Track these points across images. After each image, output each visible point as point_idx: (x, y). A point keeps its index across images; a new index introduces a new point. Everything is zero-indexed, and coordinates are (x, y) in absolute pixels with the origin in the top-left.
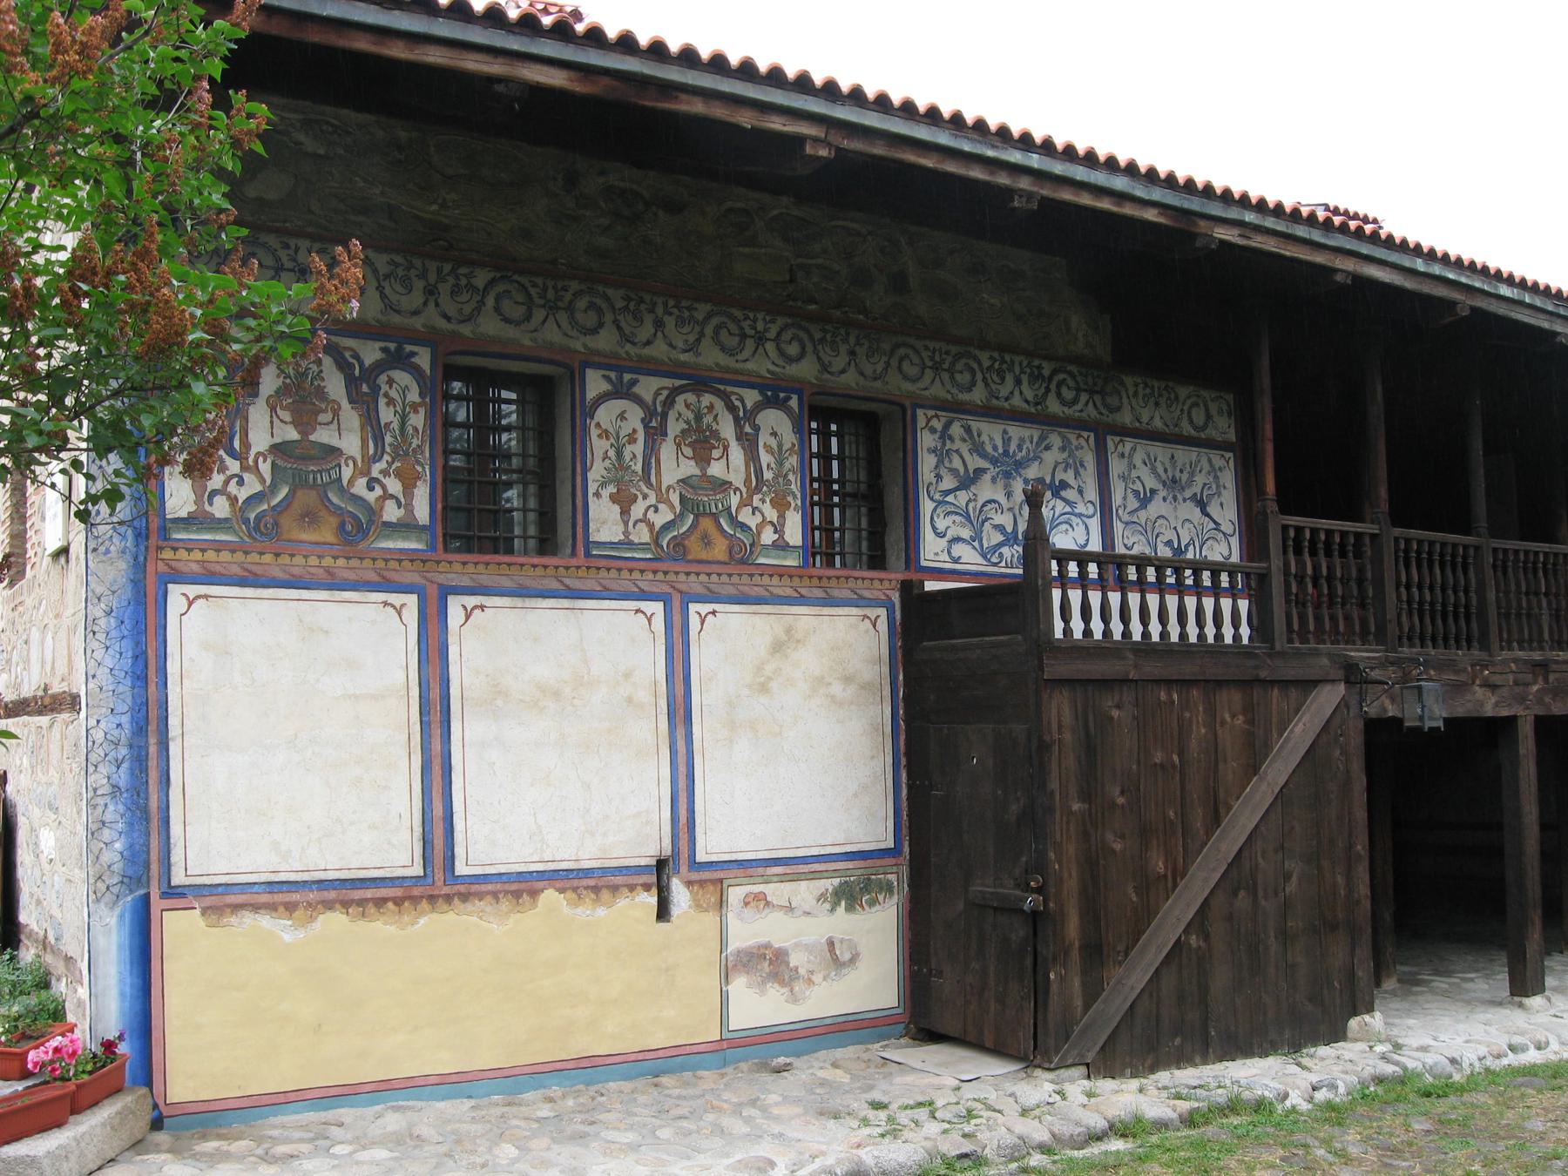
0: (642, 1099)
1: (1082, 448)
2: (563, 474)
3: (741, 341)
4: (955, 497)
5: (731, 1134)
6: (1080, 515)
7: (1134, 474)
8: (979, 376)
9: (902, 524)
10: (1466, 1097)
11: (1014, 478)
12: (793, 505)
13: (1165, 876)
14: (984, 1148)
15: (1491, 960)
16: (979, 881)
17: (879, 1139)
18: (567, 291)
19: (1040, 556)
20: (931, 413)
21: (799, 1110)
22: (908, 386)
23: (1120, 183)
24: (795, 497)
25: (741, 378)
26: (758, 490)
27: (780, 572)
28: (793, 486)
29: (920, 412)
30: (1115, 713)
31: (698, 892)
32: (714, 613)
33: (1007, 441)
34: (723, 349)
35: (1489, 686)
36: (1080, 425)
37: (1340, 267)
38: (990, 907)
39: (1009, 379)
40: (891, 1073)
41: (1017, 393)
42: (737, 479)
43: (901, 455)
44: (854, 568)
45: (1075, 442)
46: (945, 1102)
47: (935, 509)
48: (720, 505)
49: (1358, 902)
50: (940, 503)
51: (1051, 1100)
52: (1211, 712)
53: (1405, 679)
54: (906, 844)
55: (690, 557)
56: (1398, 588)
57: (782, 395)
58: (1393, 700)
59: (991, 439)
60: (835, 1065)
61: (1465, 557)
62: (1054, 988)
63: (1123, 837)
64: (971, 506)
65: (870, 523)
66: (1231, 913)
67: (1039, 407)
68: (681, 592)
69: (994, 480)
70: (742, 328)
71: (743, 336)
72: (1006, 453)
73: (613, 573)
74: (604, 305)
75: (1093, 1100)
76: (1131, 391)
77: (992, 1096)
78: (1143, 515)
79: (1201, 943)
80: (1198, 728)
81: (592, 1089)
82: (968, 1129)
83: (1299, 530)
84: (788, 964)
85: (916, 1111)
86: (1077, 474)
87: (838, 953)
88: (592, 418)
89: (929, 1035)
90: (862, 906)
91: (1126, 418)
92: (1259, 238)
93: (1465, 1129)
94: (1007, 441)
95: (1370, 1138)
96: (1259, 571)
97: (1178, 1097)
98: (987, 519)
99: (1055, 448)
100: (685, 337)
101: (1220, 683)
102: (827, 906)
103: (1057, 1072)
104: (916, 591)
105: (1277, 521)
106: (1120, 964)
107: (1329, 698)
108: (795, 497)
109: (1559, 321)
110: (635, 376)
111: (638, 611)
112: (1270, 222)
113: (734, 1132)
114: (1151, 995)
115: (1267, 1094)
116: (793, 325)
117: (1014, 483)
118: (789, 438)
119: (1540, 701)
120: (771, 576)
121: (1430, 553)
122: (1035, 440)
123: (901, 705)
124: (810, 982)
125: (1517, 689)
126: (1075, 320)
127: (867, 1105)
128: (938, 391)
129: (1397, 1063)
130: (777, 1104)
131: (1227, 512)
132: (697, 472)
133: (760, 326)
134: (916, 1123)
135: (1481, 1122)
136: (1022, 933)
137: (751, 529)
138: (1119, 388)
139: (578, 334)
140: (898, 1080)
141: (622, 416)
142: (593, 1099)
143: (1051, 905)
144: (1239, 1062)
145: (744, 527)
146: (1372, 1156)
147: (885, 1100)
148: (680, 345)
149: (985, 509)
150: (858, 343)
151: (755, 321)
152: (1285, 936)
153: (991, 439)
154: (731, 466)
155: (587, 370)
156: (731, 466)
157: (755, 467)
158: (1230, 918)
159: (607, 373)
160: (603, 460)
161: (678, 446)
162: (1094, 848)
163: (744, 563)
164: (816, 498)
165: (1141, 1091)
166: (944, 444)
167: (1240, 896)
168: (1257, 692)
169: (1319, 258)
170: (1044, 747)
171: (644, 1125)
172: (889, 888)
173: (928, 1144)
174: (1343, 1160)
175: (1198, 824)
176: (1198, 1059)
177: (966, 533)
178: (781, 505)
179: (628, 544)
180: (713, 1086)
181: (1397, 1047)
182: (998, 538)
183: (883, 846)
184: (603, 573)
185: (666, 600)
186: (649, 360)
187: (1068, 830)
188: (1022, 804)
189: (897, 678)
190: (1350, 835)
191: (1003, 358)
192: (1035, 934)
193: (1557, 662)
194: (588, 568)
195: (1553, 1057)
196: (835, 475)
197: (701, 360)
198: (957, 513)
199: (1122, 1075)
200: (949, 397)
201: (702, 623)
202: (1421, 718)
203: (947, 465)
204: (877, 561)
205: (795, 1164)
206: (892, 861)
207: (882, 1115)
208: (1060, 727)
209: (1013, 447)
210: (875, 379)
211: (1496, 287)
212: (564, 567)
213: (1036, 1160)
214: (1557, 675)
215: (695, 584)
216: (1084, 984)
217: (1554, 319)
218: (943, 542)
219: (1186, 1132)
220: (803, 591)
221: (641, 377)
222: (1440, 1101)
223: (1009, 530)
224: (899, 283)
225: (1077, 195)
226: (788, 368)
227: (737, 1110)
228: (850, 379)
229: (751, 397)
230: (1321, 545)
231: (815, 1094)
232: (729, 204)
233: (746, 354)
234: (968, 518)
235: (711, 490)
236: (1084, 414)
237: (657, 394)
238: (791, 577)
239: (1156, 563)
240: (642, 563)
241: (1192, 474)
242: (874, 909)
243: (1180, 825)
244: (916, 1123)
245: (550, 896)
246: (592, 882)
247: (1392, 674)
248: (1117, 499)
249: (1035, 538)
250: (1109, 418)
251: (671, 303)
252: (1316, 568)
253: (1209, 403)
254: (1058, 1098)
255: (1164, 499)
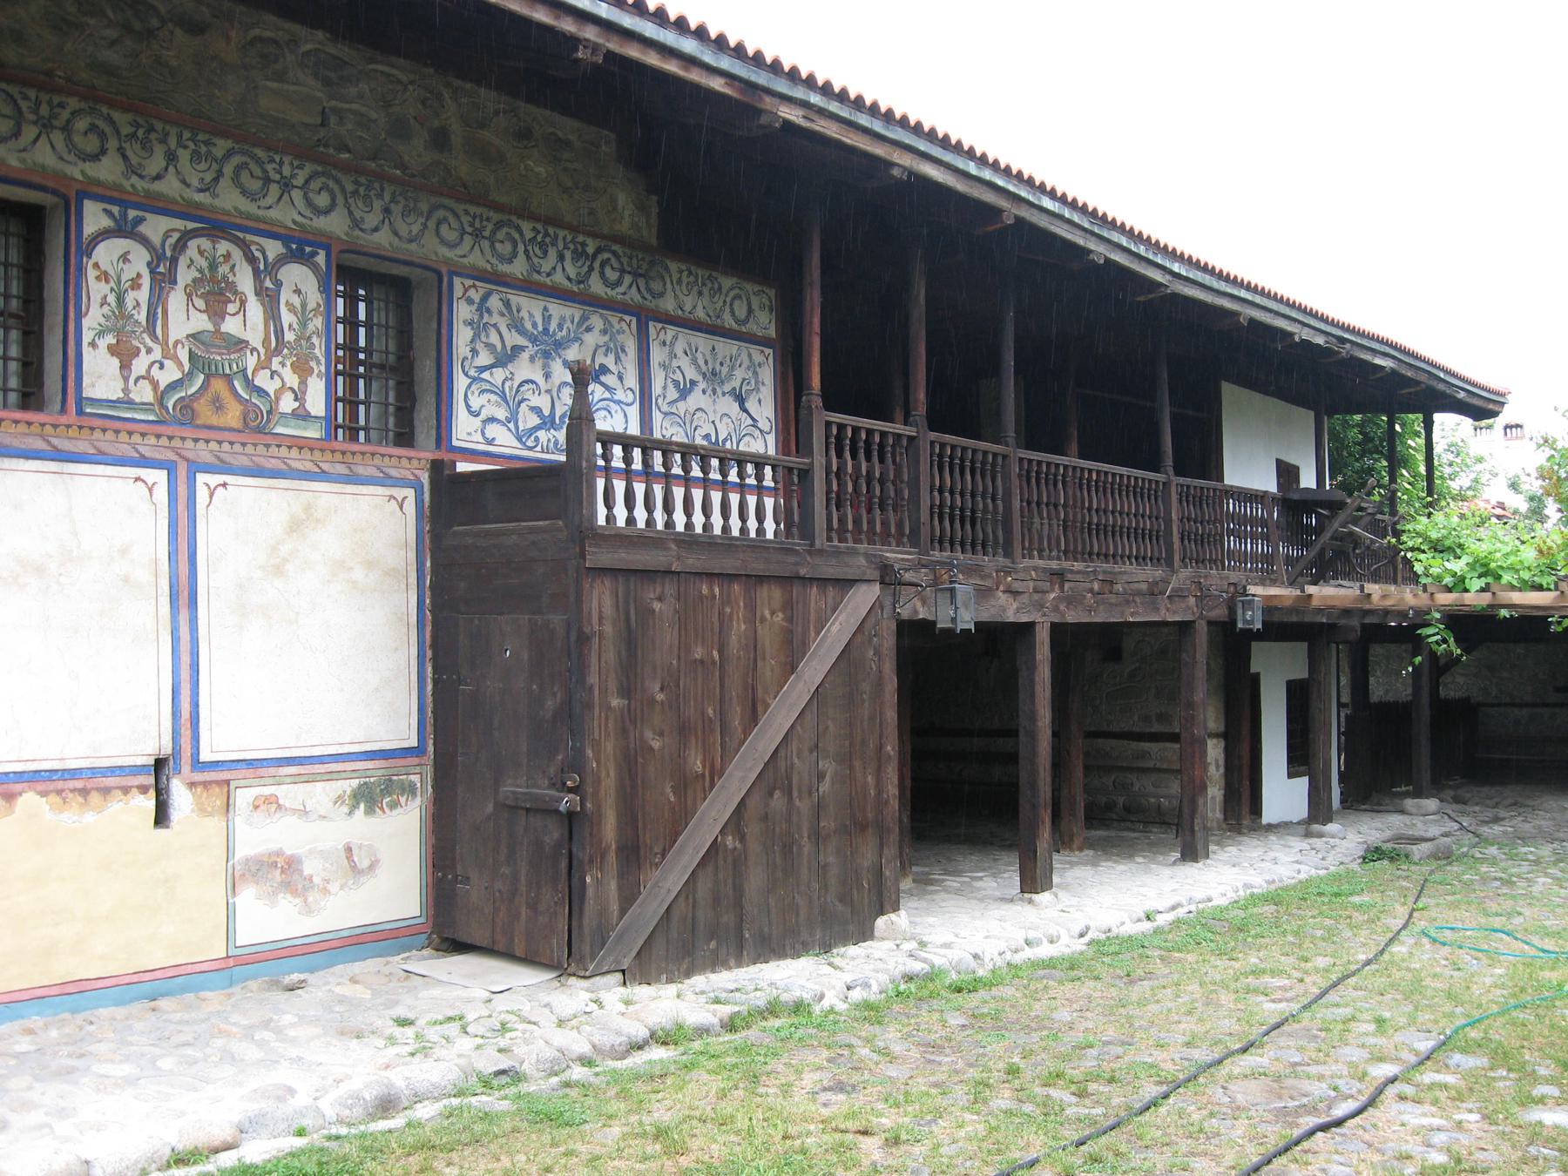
0: (138, 1026)
1: (624, 332)
2: (53, 319)
3: (264, 185)
4: (491, 374)
5: (242, 1060)
6: (619, 402)
7: (675, 363)
8: (521, 248)
9: (434, 400)
10: (994, 991)
11: (553, 359)
12: (316, 371)
13: (703, 775)
14: (522, 1063)
15: (996, 860)
16: (509, 781)
17: (409, 1058)
18: (63, 107)
19: (585, 438)
20: (469, 282)
21: (319, 1031)
22: (444, 252)
23: (689, 46)
24: (318, 363)
25: (262, 226)
26: (277, 352)
27: (300, 444)
28: (317, 351)
29: (457, 281)
30: (657, 606)
31: (201, 797)
32: (224, 485)
33: (547, 319)
34: (244, 192)
35: (1011, 592)
36: (622, 308)
37: (897, 161)
38: (522, 808)
39: (552, 253)
40: (416, 988)
41: (559, 269)
42: (255, 336)
43: (435, 325)
44: (380, 443)
45: (617, 326)
46: (476, 1015)
47: (469, 386)
48: (235, 366)
49: (887, 802)
50: (474, 379)
51: (588, 1010)
52: (752, 608)
53: (935, 583)
54: (431, 742)
55: (198, 422)
56: (931, 491)
57: (308, 249)
58: (924, 603)
59: (531, 315)
60: (353, 980)
61: (994, 465)
62: (590, 892)
63: (661, 734)
64: (508, 384)
65: (399, 397)
66: (767, 814)
67: (582, 286)
68: (187, 460)
69: (532, 359)
70: (265, 171)
71: (267, 181)
72: (546, 330)
73: (110, 435)
74: (108, 129)
75: (631, 1007)
76: (675, 276)
77: (526, 1008)
78: (682, 406)
79: (738, 845)
80: (738, 624)
81: (80, 1017)
82: (503, 1043)
83: (841, 427)
84: (301, 871)
85: (446, 1026)
86: (618, 359)
87: (356, 859)
88: (89, 256)
89: (455, 945)
90: (382, 809)
91: (669, 305)
92: (823, 122)
93: (997, 1023)
94: (547, 319)
95: (909, 1035)
96: (801, 467)
97: (717, 1001)
98: (523, 400)
99: (596, 331)
100: (201, 175)
101: (761, 579)
102: (345, 809)
103: (592, 980)
104: (447, 472)
105: (821, 419)
106: (657, 866)
107: (865, 597)
108: (318, 363)
109: (1093, 239)
110: (140, 213)
111: (137, 479)
112: (834, 107)
113: (246, 1058)
114: (687, 897)
115: (805, 996)
116: (323, 174)
117: (553, 364)
118: (314, 297)
119: (1056, 609)
120: (290, 447)
121: (962, 460)
122: (576, 320)
123: (428, 593)
124: (325, 891)
125: (1036, 597)
126: (622, 198)
127: (392, 1022)
128: (476, 259)
129: (924, 961)
130: (292, 1025)
131: (764, 409)
132: (210, 327)
133: (286, 171)
134: (447, 1039)
135: (1013, 1015)
136: (556, 835)
137: (268, 394)
138: (664, 273)
139: (76, 159)
140: (424, 994)
141: (125, 258)
142: (81, 1028)
143: (589, 805)
144: (772, 965)
145: (261, 392)
146: (915, 1053)
147: (411, 1016)
148: (195, 183)
149: (522, 389)
150: (393, 200)
151: (281, 164)
152: (817, 837)
153: (531, 315)
154: (248, 323)
155: (86, 202)
156: (248, 323)
157: (275, 326)
158: (765, 818)
159: (109, 207)
160: (102, 305)
161: (189, 296)
162: (632, 745)
163: (260, 432)
164: (340, 367)
165: (678, 996)
166: (481, 316)
167: (776, 796)
168: (796, 590)
169: (879, 150)
170: (584, 639)
171: (142, 1055)
172: (411, 790)
173: (462, 1061)
174: (888, 1059)
175: (736, 723)
176: (732, 962)
177: (501, 414)
178: (302, 370)
179: (128, 403)
180: (219, 1008)
181: (923, 944)
182: (534, 420)
183: (406, 744)
184: (98, 434)
185: (170, 468)
186: (159, 196)
187: (606, 724)
188: (558, 700)
189: (424, 564)
190: (881, 737)
191: (546, 230)
192: (571, 838)
193: (1072, 572)
194: (80, 427)
195: (1067, 951)
196: (362, 343)
197: (217, 202)
198: (492, 392)
199: (658, 981)
200: (489, 267)
201: (211, 496)
202: (954, 620)
203: (484, 339)
204: (405, 438)
205: (317, 1091)
206: (415, 761)
207: (410, 1032)
208: (601, 618)
209: (553, 326)
210: (410, 241)
211: (1039, 199)
212: (52, 425)
213: (578, 1073)
214: (1072, 584)
215: (204, 453)
216: (620, 888)
217: (1088, 236)
218: (477, 422)
219: (728, 1037)
220: (325, 466)
221: (147, 215)
222: (971, 995)
223: (546, 412)
224: (440, 139)
225: (644, 53)
226: (315, 219)
227: (248, 1034)
228: (383, 238)
229: (274, 248)
230: (862, 444)
231: (333, 1012)
232: (256, 32)
233: (269, 200)
234: (504, 398)
235: (225, 348)
236: (627, 297)
237: (167, 235)
238: (311, 450)
239: (702, 452)
240: (143, 425)
241: (732, 368)
242: (395, 812)
243: (718, 724)
244: (447, 1039)
245: (29, 800)
246: (79, 784)
247: (922, 576)
248: (657, 388)
249: (580, 418)
250: (651, 304)
251: (186, 135)
252: (857, 468)
253: (752, 297)
254: (595, 1007)
255: (704, 392)
